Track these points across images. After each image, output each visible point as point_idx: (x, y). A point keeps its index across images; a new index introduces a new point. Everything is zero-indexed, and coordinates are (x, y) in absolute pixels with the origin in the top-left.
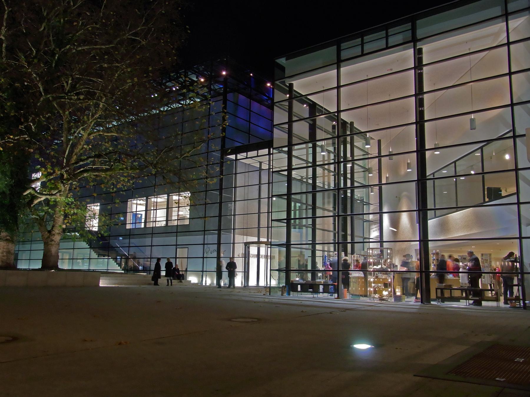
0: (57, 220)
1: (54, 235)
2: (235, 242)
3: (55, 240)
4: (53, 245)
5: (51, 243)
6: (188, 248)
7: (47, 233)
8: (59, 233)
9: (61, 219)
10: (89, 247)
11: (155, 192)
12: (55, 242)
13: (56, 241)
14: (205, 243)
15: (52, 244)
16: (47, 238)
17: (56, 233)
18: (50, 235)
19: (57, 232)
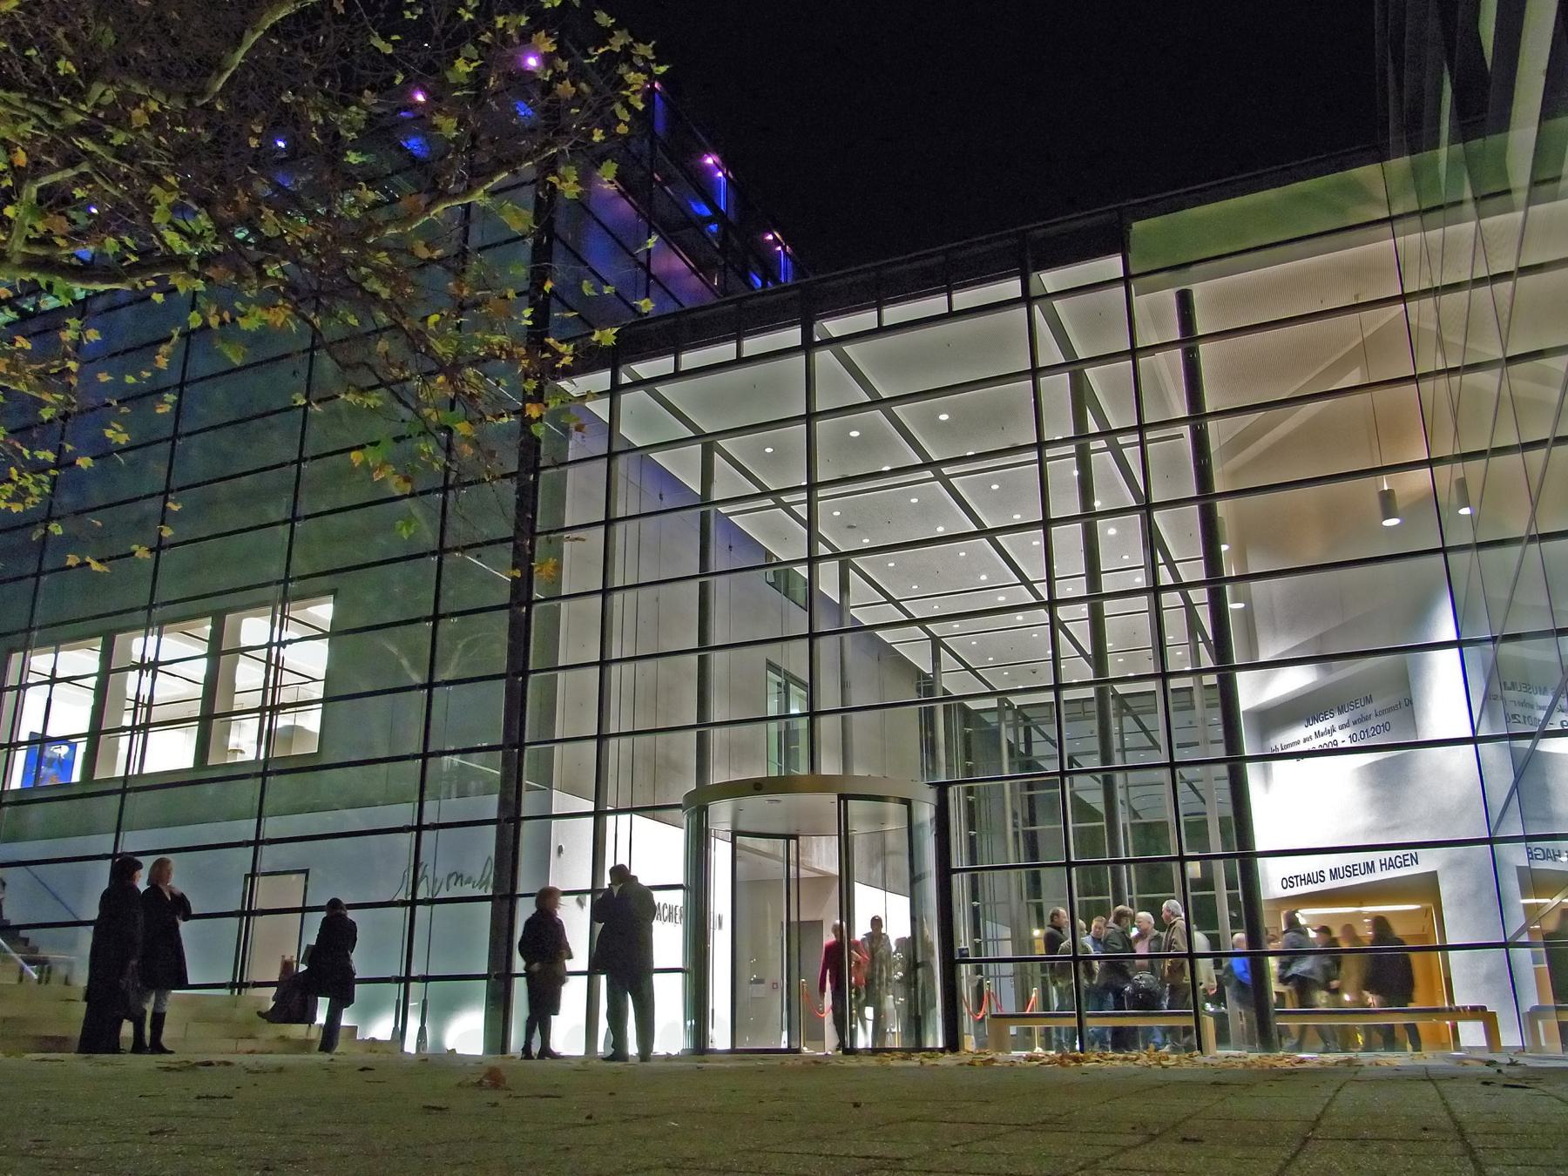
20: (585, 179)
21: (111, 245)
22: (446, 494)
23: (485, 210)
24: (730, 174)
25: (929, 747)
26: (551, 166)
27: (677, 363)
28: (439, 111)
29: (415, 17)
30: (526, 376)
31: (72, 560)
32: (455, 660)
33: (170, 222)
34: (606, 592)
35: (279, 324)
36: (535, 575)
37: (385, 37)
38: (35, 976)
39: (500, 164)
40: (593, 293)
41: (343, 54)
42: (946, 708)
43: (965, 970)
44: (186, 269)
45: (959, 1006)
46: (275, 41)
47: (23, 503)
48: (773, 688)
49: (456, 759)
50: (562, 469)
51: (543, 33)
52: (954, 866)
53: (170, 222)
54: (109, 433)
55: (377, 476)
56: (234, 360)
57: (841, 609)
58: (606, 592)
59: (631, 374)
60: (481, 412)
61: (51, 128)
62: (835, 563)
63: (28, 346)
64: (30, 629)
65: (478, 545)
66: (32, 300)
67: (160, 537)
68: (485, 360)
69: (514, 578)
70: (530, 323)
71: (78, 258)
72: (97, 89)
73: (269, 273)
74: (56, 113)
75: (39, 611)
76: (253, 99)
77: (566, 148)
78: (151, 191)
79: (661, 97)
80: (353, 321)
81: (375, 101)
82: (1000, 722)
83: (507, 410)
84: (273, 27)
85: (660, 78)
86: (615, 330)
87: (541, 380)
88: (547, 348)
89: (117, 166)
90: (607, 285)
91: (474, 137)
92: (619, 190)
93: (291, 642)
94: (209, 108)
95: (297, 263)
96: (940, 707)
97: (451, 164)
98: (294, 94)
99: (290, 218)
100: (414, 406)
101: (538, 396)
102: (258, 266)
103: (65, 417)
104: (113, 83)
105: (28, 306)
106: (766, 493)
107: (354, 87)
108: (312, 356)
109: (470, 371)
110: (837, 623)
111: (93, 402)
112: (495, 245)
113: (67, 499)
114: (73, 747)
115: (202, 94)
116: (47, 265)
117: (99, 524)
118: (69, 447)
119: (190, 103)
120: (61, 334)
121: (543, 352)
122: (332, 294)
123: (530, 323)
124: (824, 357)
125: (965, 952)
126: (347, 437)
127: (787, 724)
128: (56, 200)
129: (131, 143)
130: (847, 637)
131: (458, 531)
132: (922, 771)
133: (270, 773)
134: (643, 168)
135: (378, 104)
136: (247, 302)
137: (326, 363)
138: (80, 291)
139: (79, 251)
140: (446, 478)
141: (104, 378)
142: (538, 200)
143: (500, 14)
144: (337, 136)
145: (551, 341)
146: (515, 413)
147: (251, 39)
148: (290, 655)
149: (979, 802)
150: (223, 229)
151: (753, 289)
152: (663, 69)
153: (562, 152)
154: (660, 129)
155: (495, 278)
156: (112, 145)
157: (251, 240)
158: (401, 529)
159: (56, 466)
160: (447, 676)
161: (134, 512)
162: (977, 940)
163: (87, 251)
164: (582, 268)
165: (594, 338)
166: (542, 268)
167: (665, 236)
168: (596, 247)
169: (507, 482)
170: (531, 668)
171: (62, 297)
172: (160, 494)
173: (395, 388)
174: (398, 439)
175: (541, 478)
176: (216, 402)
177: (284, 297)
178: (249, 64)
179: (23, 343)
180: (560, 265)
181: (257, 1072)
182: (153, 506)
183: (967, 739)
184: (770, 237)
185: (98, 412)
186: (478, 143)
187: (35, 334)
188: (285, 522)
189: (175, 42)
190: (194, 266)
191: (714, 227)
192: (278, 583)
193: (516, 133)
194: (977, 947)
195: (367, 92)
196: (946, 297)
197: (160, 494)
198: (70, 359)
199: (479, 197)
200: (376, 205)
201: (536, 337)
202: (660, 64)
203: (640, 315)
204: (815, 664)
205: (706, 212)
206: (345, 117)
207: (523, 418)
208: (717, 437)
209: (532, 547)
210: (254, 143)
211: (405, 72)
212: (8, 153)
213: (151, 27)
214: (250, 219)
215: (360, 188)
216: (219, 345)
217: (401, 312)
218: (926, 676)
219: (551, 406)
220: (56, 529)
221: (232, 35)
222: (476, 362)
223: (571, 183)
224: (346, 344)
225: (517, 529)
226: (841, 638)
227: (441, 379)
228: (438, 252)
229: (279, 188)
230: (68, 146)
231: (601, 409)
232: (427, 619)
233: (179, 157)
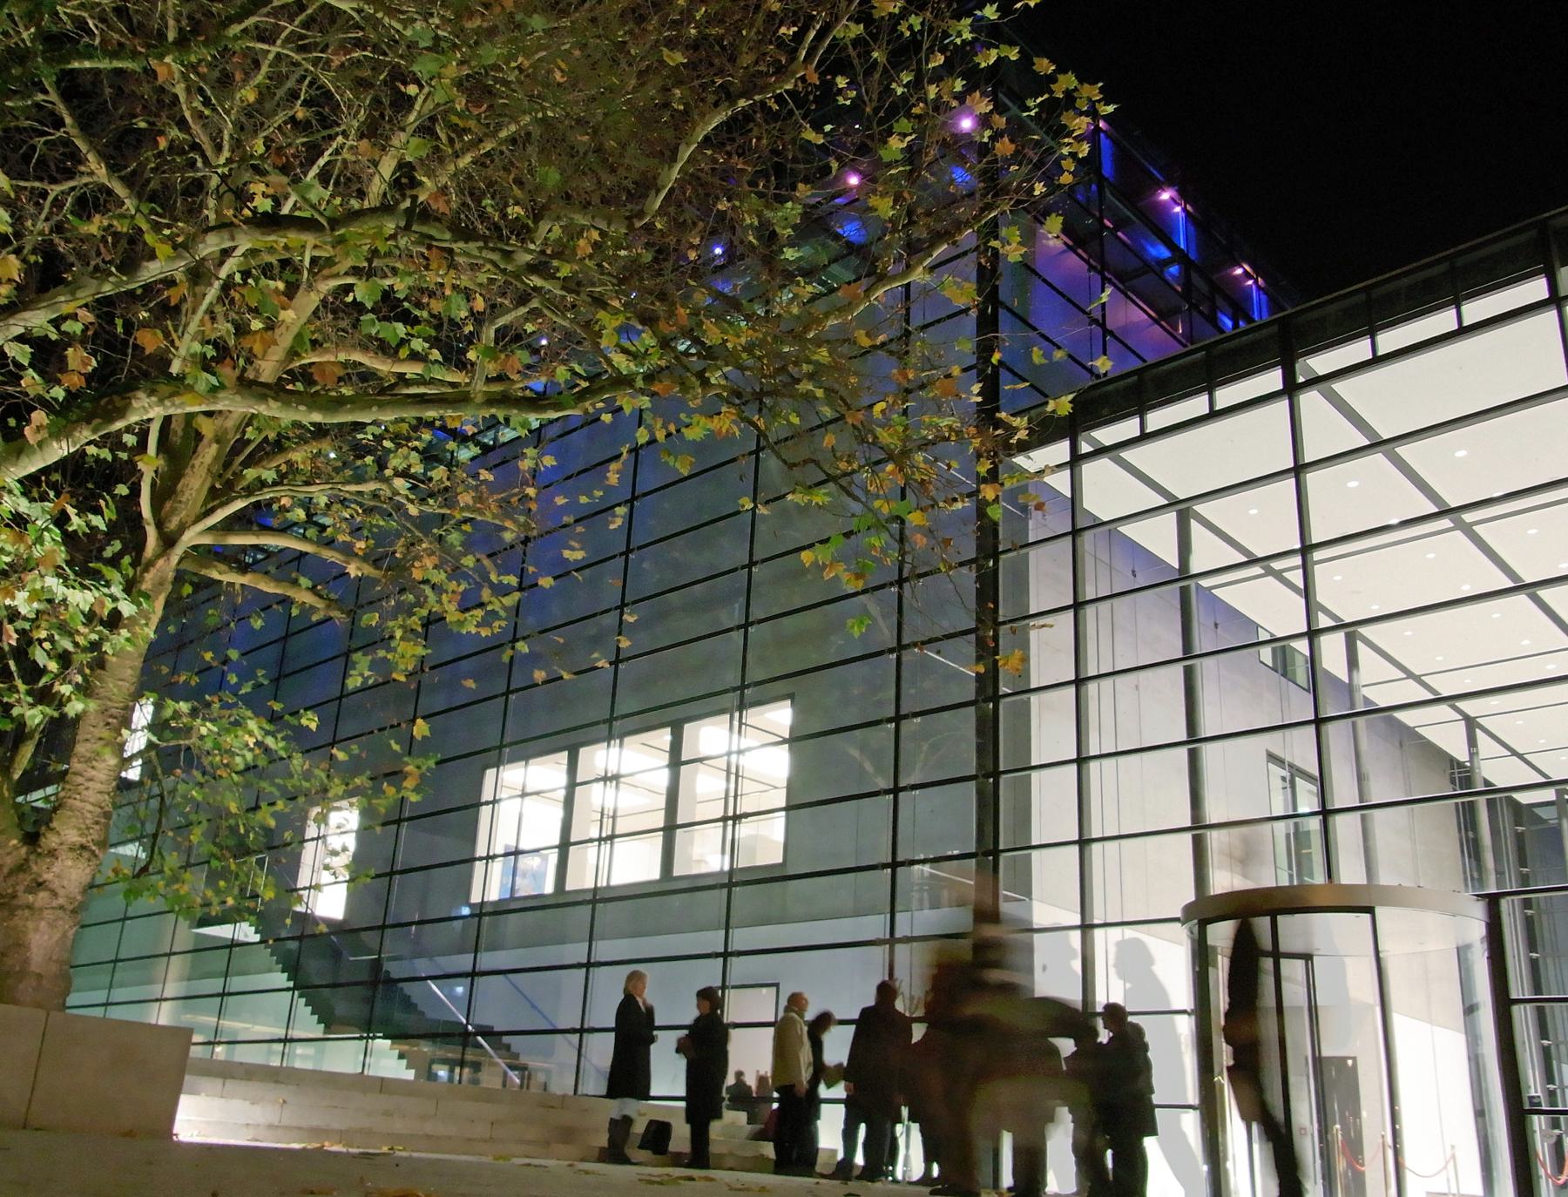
0: (81, 775)
1: (52, 853)
2: (1092, 918)
3: (56, 885)
4: (41, 910)
5: (31, 898)
6: (777, 985)
7: (15, 842)
8: (83, 847)
9: (99, 771)
10: (291, 984)
11: (620, 634)
12: (55, 894)
13: (61, 892)
14: (898, 935)
15: (37, 905)
16: (11, 873)
17: (64, 847)
18: (32, 857)
19: (73, 836)
20: (1029, 238)
21: (562, 373)
22: (901, 587)
23: (926, 290)
24: (1189, 207)
25: (1473, 849)
26: (993, 230)
27: (1142, 425)
28: (874, 192)
29: (848, 102)
30: (979, 455)
31: (540, 675)
32: (919, 766)
33: (618, 345)
34: (1079, 682)
35: (724, 431)
36: (1001, 670)
37: (818, 128)
38: (518, 1081)
39: (937, 237)
40: (1044, 361)
41: (775, 152)
42: (1490, 803)
43: (1538, 1123)
44: (632, 386)
45: (1533, 1167)
46: (709, 152)
47: (491, 627)
48: (1277, 784)
49: (927, 868)
50: (1023, 551)
51: (978, 93)
52: (1514, 996)
53: (618, 345)
54: (567, 554)
55: (828, 575)
56: (682, 471)
57: (1350, 689)
58: (1079, 682)
59: (1092, 441)
60: (933, 499)
61: (504, 271)
62: (1340, 637)
63: (491, 478)
64: (500, 747)
65: (937, 640)
66: (491, 434)
67: (618, 649)
68: (933, 442)
69: (977, 673)
70: (979, 399)
71: (531, 390)
72: (544, 227)
73: (713, 381)
74: (507, 255)
75: (508, 732)
76: (690, 213)
77: (1007, 208)
78: (598, 316)
79: (1108, 136)
80: (795, 420)
81: (809, 193)
82: (1559, 818)
83: (961, 495)
84: (707, 138)
85: (1107, 118)
86: (1071, 397)
87: (994, 456)
88: (998, 424)
89: (564, 297)
90: (1059, 348)
91: (910, 213)
92: (1065, 243)
93: (749, 749)
94: (649, 228)
95: (741, 368)
96: (1481, 801)
97: (889, 246)
98: (729, 201)
99: (730, 324)
100: (864, 500)
101: (993, 476)
102: (701, 375)
103: (526, 541)
104: (558, 218)
105: (488, 439)
106: (1254, 561)
107: (788, 181)
108: (757, 459)
109: (919, 457)
110: (1348, 705)
111: (550, 525)
112: (938, 321)
113: (529, 623)
114: (545, 859)
115: (641, 214)
116: (504, 400)
117: (562, 641)
118: (531, 569)
119: (631, 227)
120: (520, 463)
121: (995, 429)
122: (773, 393)
123: (979, 399)
124: (1310, 401)
125: (1535, 1101)
126: (796, 537)
127: (1296, 825)
128: (510, 338)
129: (575, 273)
130: (1361, 721)
131: (916, 628)
132: (1466, 879)
133: (737, 884)
134: (1093, 216)
135: (813, 195)
136: (690, 412)
137: (771, 463)
138: (534, 420)
139: (531, 383)
140: (901, 570)
141: (560, 501)
142: (980, 267)
143: (931, 82)
144: (774, 234)
145: (1003, 415)
146: (969, 495)
147: (685, 153)
148: (748, 763)
149: (1540, 915)
150: (665, 344)
151: (1222, 332)
152: (1110, 109)
153: (1003, 213)
154: (1107, 169)
155: (940, 356)
156: (559, 278)
157: (693, 351)
158: (852, 627)
159: (520, 589)
160: (913, 780)
161: (590, 628)
162: (1551, 1087)
163: (539, 382)
164: (1032, 334)
165: (1050, 408)
166: (989, 339)
167: (1120, 286)
168: (1045, 310)
169: (964, 570)
170: (1001, 769)
171: (519, 428)
172: (616, 608)
173: (843, 482)
174: (848, 535)
175: (1001, 563)
176: (662, 514)
177: (729, 403)
178: (688, 178)
179: (485, 475)
180: (1007, 332)
181: (740, 1190)
182: (610, 620)
183: (1520, 839)
184: (1239, 271)
185: (556, 533)
186: (915, 218)
187: (495, 466)
188: (739, 627)
189: (613, 170)
190: (640, 383)
191: (1174, 269)
192: (734, 689)
193: (954, 201)
194: (1552, 1095)
195: (801, 186)
196: (1454, 311)
197: (616, 608)
198: (528, 485)
199: (918, 276)
200: (815, 298)
201: (987, 414)
202: (1107, 104)
203: (1098, 376)
204: (1324, 756)
205: (1164, 253)
206: (780, 214)
207: (978, 501)
208: (1195, 502)
209: (996, 638)
210: (692, 255)
211: (839, 158)
212: (468, 301)
213: (592, 158)
214: (692, 330)
215: (798, 284)
216: (665, 458)
217: (846, 404)
218: (1460, 765)
219: (1008, 485)
220: (522, 647)
221: (668, 153)
222: (925, 445)
223: (1014, 245)
224: (790, 443)
225: (979, 620)
226: (1354, 724)
227: (890, 467)
228: (881, 338)
229: (719, 295)
230: (519, 285)
231: (1060, 482)
232: (889, 720)
233: (621, 282)
